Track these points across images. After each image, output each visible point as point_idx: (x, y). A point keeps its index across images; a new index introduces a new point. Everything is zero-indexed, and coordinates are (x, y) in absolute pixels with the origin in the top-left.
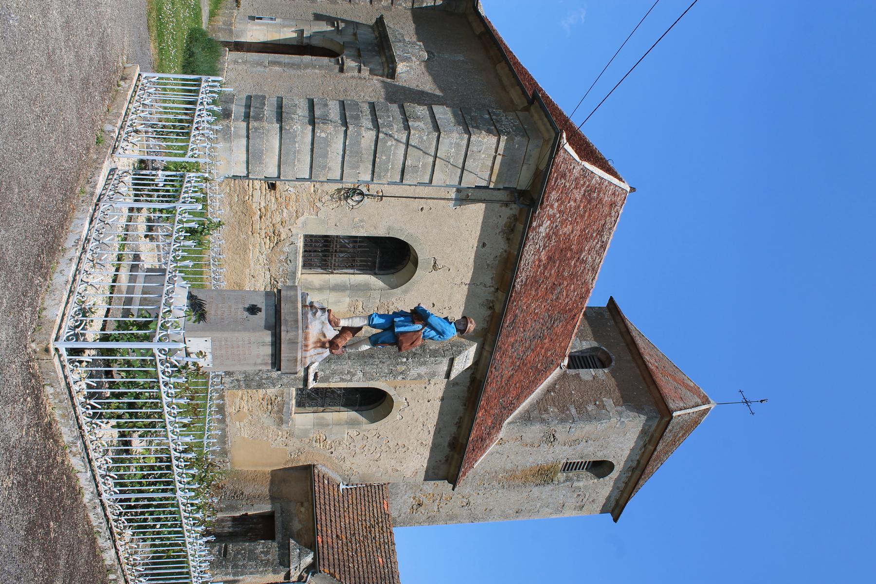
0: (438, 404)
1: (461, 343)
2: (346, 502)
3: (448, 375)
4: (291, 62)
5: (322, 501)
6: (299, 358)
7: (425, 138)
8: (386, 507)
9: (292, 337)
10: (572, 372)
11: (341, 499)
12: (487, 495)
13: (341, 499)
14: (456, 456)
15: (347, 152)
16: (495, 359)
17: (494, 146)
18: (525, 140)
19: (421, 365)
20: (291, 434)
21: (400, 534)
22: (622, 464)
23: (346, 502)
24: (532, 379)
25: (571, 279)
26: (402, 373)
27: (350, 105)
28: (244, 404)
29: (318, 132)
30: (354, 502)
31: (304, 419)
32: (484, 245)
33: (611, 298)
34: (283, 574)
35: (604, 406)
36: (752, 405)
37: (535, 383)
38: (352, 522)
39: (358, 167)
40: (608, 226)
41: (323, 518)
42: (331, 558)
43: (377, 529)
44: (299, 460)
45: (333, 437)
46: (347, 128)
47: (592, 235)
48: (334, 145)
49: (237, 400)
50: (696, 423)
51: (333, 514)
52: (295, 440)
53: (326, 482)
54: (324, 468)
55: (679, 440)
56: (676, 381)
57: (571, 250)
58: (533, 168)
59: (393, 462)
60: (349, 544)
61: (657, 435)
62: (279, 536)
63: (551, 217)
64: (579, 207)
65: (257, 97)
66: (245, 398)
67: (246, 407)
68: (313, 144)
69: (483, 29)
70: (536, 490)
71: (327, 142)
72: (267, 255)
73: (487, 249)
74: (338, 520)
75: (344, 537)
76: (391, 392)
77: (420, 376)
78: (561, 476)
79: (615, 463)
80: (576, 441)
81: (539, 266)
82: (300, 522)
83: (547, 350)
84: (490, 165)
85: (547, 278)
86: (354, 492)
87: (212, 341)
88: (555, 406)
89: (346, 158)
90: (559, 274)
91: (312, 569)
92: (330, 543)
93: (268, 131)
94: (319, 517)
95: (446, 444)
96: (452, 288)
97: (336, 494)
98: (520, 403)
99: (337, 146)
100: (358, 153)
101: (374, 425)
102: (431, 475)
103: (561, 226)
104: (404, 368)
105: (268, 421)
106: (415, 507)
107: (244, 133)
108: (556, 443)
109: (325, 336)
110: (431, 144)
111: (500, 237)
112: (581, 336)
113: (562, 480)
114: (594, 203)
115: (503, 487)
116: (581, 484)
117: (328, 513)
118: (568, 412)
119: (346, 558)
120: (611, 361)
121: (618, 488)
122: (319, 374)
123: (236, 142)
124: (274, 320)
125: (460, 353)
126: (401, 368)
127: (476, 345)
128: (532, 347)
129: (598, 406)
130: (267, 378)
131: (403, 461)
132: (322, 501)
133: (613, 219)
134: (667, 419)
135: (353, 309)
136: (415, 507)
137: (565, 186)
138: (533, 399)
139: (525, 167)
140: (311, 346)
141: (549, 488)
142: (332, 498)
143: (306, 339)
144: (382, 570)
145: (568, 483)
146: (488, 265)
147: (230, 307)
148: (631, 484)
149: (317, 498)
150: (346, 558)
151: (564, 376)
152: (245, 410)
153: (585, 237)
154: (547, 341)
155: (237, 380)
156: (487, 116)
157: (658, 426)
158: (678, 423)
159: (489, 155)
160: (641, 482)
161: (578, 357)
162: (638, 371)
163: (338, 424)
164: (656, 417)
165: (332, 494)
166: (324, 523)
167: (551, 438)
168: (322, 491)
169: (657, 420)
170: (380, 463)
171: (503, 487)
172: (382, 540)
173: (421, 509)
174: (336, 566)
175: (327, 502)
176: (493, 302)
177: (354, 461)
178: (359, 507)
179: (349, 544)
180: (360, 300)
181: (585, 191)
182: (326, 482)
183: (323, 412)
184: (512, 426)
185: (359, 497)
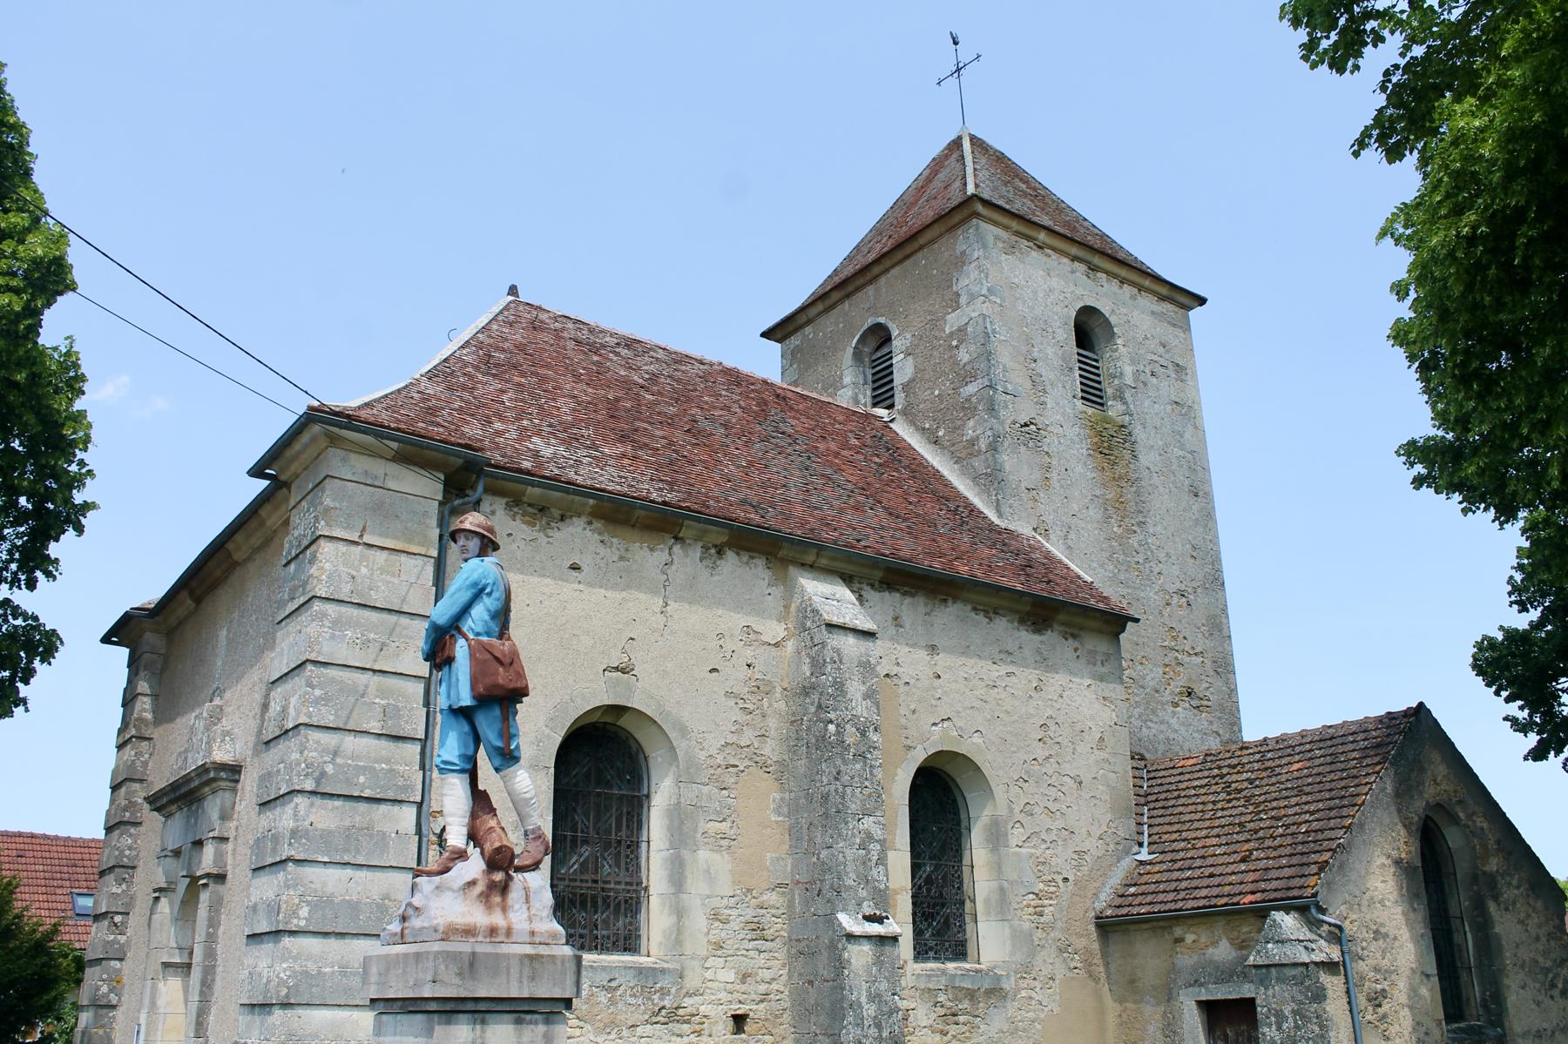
2: (1176, 846)
5: (1171, 896)
6: (529, 950)
7: (318, 692)
8: (1191, 762)
9: (454, 969)
10: (899, 399)
11: (1169, 856)
12: (1162, 556)
13: (1169, 856)
14: (1062, 617)
15: (346, 859)
17: (342, 547)
20: (1026, 969)
21: (1252, 732)
23: (1176, 846)
24: (905, 473)
26: (863, 734)
29: (295, 924)
31: (991, 941)
32: (575, 567)
33: (764, 335)
34: (1325, 978)
35: (959, 330)
36: (963, 60)
37: (918, 467)
38: (1216, 831)
39: (383, 835)
40: (584, 335)
41: (1204, 892)
42: (1287, 872)
43: (1234, 777)
45: (1029, 877)
47: (594, 363)
48: (330, 889)
50: (1000, 159)
51: (1197, 873)
53: (1132, 890)
54: (1103, 896)
55: (1035, 189)
57: (617, 400)
58: (393, 468)
59: (1082, 748)
60: (1261, 834)
61: (1014, 224)
62: (1247, 991)
63: (524, 435)
68: (326, 934)
69: (184, 594)
70: (1146, 458)
71: (322, 903)
73: (585, 561)
74: (1210, 861)
75: (1246, 847)
76: (919, 757)
78: (1114, 409)
82: (1215, 944)
83: (845, 445)
84: (385, 554)
85: (671, 443)
91: (1307, 909)
92: (1256, 876)
94: (1202, 903)
95: (1037, 638)
97: (1157, 868)
98: (958, 495)
99: (331, 880)
101: (999, 791)
102: (1111, 668)
103: (551, 415)
104: (850, 729)
106: (1195, 703)
109: (472, 883)
110: (333, 680)
111: (557, 534)
112: (835, 385)
113: (1121, 407)
114: (520, 358)
116: (1128, 370)
117: (1194, 883)
119: (1289, 840)
120: (879, 325)
124: (419, 1017)
125: (815, 612)
127: (803, 581)
129: (961, 342)
130: (879, 1026)
131: (1078, 727)
132: (1171, 896)
133: (570, 325)
134: (980, 208)
135: (725, 843)
136: (1195, 703)
137: (460, 410)
138: (953, 471)
139: (391, 484)
140: (498, 919)
141: (1139, 433)
142: (1165, 876)
143: (469, 932)
144: (1317, 762)
145: (1127, 395)
146: (621, 558)
148: (1123, 272)
150: (1289, 840)
153: (597, 376)
157: (996, 223)
158: (995, 189)
159: (363, 557)
160: (1121, 256)
161: (874, 389)
162: (895, 271)
163: (998, 867)
166: (1215, 891)
167: (1030, 430)
168: (1149, 898)
169: (983, 225)
172: (1256, 766)
173: (1199, 689)
174: (1305, 860)
175: (1174, 885)
176: (705, 548)
177: (1084, 831)
178: (1187, 817)
179: (1261, 834)
180: (703, 826)
181: (484, 374)
182: (1132, 890)
184: (1006, 510)
185: (1167, 819)
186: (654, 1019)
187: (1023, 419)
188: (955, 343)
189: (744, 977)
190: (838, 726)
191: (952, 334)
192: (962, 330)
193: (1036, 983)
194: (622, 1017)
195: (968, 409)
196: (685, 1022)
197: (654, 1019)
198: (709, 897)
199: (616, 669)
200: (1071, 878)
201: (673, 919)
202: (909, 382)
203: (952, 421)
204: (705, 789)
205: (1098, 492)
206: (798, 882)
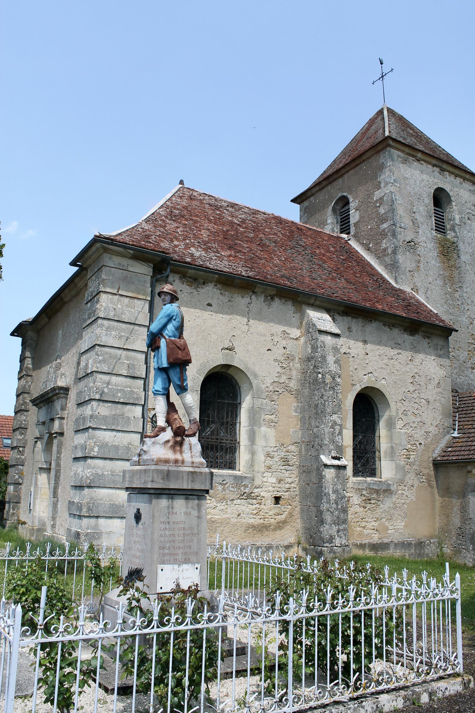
0: (369, 347)
1: (306, 324)
3: (337, 335)
4: (54, 478)
5: (467, 453)
6: (191, 469)
11: (467, 435)
12: (469, 302)
13: (467, 435)
15: (113, 428)
16: (323, 294)
17: (110, 296)
18: (104, 269)
19: (325, 361)
20: (401, 482)
22: (436, 181)
25: (259, 231)
26: (334, 379)
27: (77, 425)
28: (369, 526)
30: (470, 423)
32: (209, 305)
33: (292, 201)
35: (380, 199)
36: (385, 71)
40: (213, 202)
44: (429, 475)
45: (404, 442)
46: (89, 427)
48: (106, 440)
49: (366, 532)
52: (407, 479)
53: (450, 449)
54: (436, 452)
55: (417, 133)
56: (362, 139)
57: (228, 231)
58: (131, 262)
59: (430, 387)
61: (407, 150)
64: (185, 224)
65: (69, 509)
66: (363, 524)
67: (373, 523)
68: (105, 459)
71: (103, 446)
72: (218, 502)
73: (214, 302)
76: (358, 389)
77: (337, 362)
78: (450, 235)
79: (437, 187)
80: (414, 221)
81: (235, 256)
83: (328, 251)
85: (251, 250)
86: (461, 423)
87: (163, 563)
88: (381, 242)
89: (119, 428)
90: (250, 241)
93: (92, 499)
95: (411, 338)
96: (252, 333)
97: (461, 440)
100: (115, 418)
101: (392, 404)
102: (443, 352)
103: (199, 238)
104: (328, 376)
105: (387, 504)
107: (93, 521)
108: (415, 240)
109: (168, 441)
110: (107, 353)
112: (323, 223)
113: (453, 234)
114: (185, 212)
115: (460, 287)
116: (457, 217)
118: (386, 230)
121: (461, 183)
122: (334, 455)
123: (102, 529)
124: (146, 495)
125: (314, 325)
126: (328, 379)
127: (308, 311)
128: (321, 263)
129: (381, 204)
130: (337, 504)
131: (429, 377)
132: (467, 453)
133: (207, 198)
134: (391, 142)
135: (273, 424)
137: (159, 236)
138: (376, 262)
139: (130, 269)
140: (178, 456)
141: (461, 246)
143: (167, 461)
147: (135, 542)
148: (457, 172)
149: (463, 457)
151: (356, 237)
152: (376, 524)
153: (219, 220)
154: (318, 251)
155: (338, 531)
156: (89, 304)
157: (398, 149)
158: (398, 133)
159: (119, 301)
160: (456, 164)
161: (341, 226)
162: (351, 172)
163: (391, 438)
164: (390, 151)
165: (461, 444)
167: (411, 245)
168: (457, 453)
169: (392, 150)
170: (431, 400)
171: (460, 287)
175: (468, 448)
177: (429, 423)
180: (263, 417)
182: (450, 449)
183: (380, 452)
184: (399, 280)
185: (467, 419)
186: (241, 497)
187: (408, 239)
188: (378, 205)
189: (280, 481)
190: (322, 375)
191: (377, 200)
192: (382, 199)
193: (406, 488)
194: (228, 496)
195: (383, 234)
196: (254, 499)
197: (241, 497)
198: (265, 447)
199: (227, 349)
200: (423, 443)
201: (250, 456)
202: (357, 222)
203: (376, 240)
204: (265, 401)
205: (441, 273)
206: (304, 442)
